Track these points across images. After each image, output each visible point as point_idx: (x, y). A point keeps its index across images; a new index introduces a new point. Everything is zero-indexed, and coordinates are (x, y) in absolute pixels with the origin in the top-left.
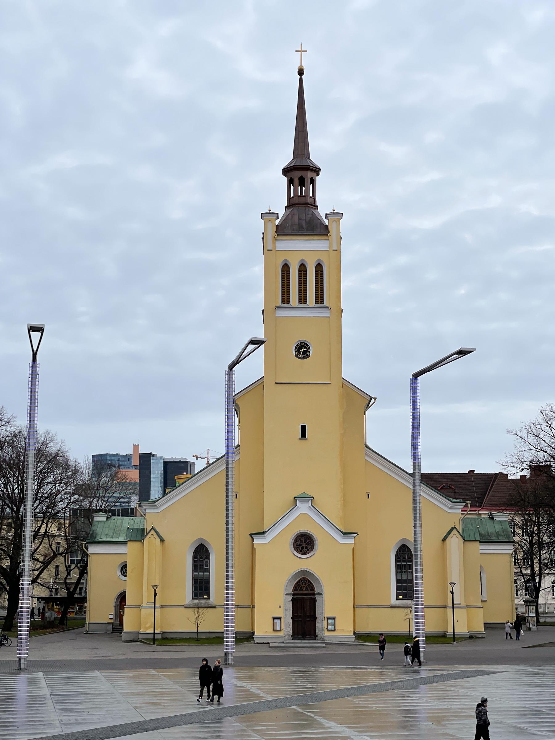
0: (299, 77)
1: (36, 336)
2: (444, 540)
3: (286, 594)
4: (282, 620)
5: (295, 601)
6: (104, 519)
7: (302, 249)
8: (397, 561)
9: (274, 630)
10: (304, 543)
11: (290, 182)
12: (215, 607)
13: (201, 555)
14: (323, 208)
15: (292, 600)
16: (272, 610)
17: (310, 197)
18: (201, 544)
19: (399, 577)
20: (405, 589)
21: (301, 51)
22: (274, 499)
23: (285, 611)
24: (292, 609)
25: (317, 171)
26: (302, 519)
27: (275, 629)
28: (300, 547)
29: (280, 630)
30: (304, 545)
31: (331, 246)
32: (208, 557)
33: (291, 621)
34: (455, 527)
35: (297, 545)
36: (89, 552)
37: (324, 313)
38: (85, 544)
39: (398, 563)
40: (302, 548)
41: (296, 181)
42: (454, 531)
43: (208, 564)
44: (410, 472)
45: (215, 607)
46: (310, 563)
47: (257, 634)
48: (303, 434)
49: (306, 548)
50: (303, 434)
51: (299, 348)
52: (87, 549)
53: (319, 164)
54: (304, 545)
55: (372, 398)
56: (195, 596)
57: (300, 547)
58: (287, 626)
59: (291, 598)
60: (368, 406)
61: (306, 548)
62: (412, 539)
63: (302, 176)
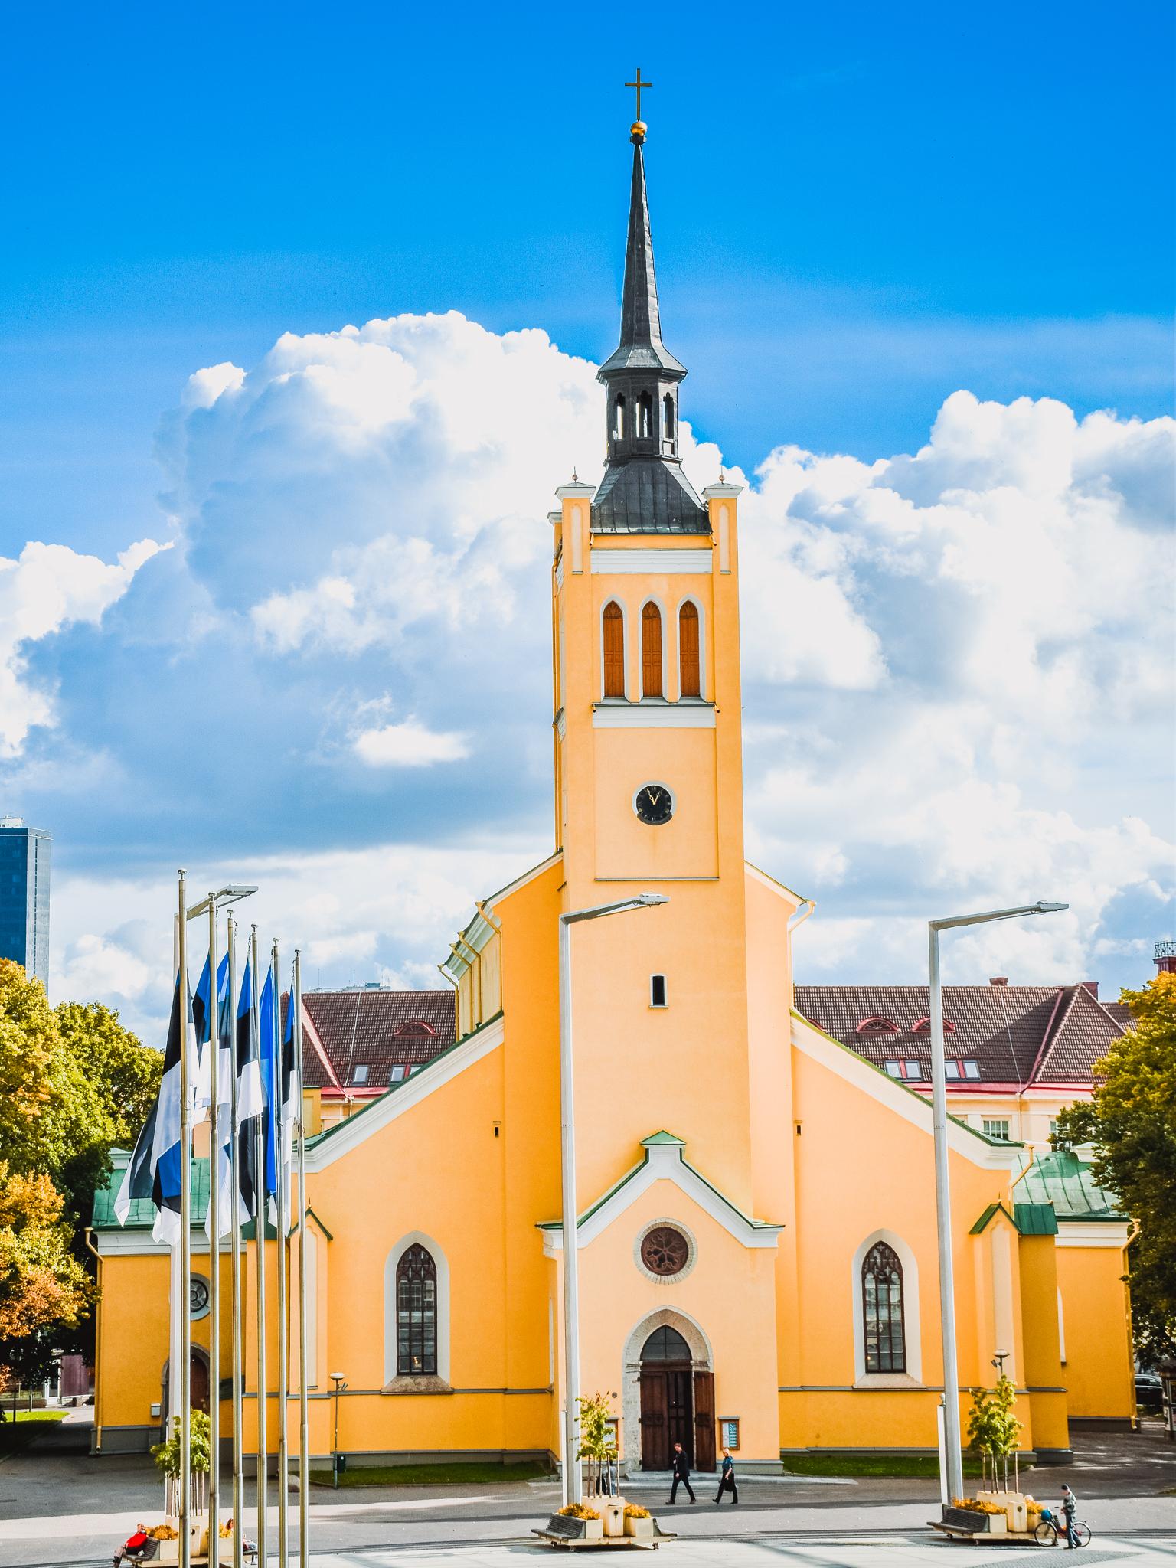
2: (972, 1232)
4: (621, 1423)
5: (646, 1379)
7: (649, 568)
10: (666, 1250)
12: (453, 1392)
13: (416, 1270)
16: (598, 1378)
18: (416, 1245)
20: (417, 1353)
22: (588, 1152)
23: (625, 1405)
24: (639, 1400)
26: (658, 1196)
31: (715, 563)
32: (432, 1275)
33: (639, 1427)
34: (1000, 1206)
35: (649, 1253)
36: (98, 1254)
37: (703, 718)
38: (91, 1232)
42: (999, 1214)
45: (453, 1392)
48: (659, 997)
50: (659, 997)
51: (643, 800)
52: (94, 1240)
54: (665, 1252)
58: (386, 1373)
59: (638, 1375)
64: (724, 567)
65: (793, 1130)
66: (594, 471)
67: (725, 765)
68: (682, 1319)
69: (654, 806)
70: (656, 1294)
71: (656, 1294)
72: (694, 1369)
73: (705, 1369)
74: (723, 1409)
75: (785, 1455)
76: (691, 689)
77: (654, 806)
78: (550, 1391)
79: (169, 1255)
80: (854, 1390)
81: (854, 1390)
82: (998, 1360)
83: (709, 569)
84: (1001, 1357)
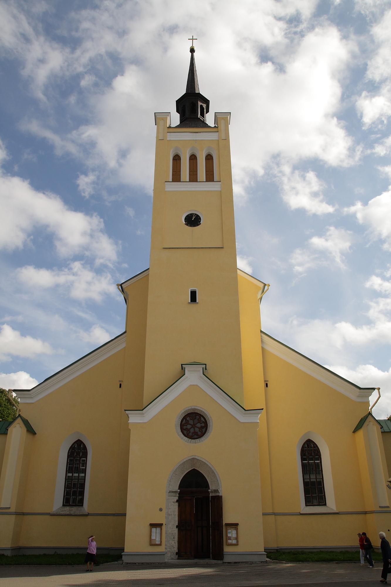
0: (191, 54)
2: (354, 432)
4: (164, 527)
7: (193, 194)
9: (151, 545)
12: (87, 515)
15: (177, 501)
21: (193, 39)
22: (154, 372)
23: (168, 513)
26: (190, 391)
27: (153, 543)
29: (160, 545)
32: (85, 454)
33: (176, 531)
43: (85, 463)
55: (265, 285)
56: (67, 502)
58: (169, 540)
59: (177, 498)
60: (263, 292)
65: (263, 385)
68: (204, 464)
69: (193, 220)
70: (186, 451)
71: (186, 451)
72: (211, 495)
73: (217, 494)
74: (228, 517)
75: (265, 550)
76: (210, 178)
77: (193, 220)
78: (125, 515)
83: (217, 139)
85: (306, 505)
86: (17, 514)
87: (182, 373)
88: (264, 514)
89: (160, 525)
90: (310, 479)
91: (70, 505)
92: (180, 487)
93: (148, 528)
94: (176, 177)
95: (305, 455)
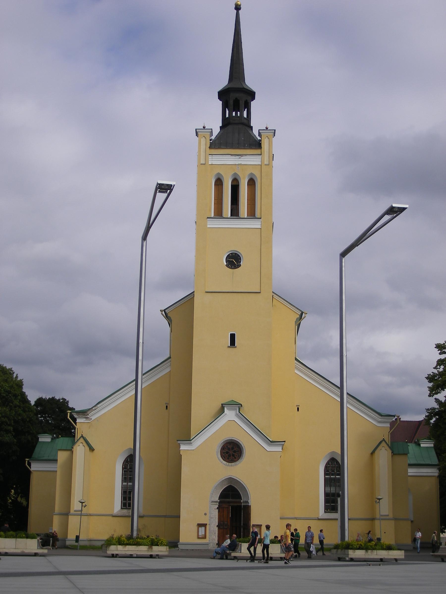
1: (202, 530)
2: (373, 453)
3: (212, 502)
6: (49, 440)
7: (230, 162)
8: (325, 474)
9: (199, 538)
10: (232, 451)
11: (225, 106)
14: (258, 122)
16: (198, 511)
17: (245, 118)
19: (328, 489)
20: (333, 501)
23: (212, 518)
24: (217, 517)
25: (252, 95)
26: (229, 425)
28: (227, 450)
29: (205, 537)
30: (231, 452)
33: (217, 529)
34: (384, 440)
35: (224, 453)
37: (255, 224)
39: (326, 477)
40: (229, 456)
41: (231, 102)
42: (384, 442)
44: (339, 385)
46: (238, 471)
47: (181, 541)
49: (233, 455)
52: (29, 464)
53: (254, 89)
54: (231, 452)
57: (227, 450)
59: (217, 506)
61: (233, 455)
62: (339, 452)
63: (236, 99)
64: (266, 162)
66: (216, 125)
67: (265, 239)
69: (234, 261)
70: (226, 471)
71: (226, 471)
72: (243, 504)
73: (248, 504)
76: (252, 214)
77: (234, 261)
79: (57, 471)
80: (319, 519)
81: (319, 519)
82: (378, 501)
84: (379, 499)
85: (325, 512)
86: (323, 551)
87: (221, 411)
88: (281, 518)
89: (205, 525)
90: (330, 491)
91: (126, 509)
92: (220, 498)
93: (196, 528)
94: (219, 214)
95: (328, 471)
